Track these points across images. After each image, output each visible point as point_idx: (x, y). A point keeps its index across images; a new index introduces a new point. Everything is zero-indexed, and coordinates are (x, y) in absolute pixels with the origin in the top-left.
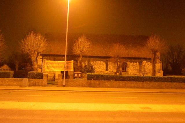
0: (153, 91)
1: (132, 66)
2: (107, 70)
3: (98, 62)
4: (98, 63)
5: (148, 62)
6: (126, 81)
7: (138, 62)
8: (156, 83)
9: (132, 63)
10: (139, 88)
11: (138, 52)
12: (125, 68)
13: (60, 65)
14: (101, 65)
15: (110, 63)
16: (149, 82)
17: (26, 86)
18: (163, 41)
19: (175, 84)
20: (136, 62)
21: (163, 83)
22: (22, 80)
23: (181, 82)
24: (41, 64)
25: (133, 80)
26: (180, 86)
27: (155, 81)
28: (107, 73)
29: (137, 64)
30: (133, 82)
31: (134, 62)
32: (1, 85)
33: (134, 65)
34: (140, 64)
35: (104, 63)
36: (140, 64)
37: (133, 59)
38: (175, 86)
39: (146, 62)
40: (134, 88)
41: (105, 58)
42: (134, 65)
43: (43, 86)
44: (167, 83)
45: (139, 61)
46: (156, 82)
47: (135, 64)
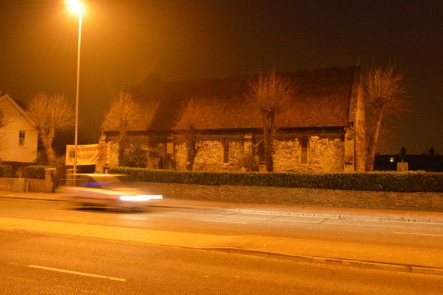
0: (183, 204)
1: (283, 148)
2: (226, 160)
3: (208, 142)
4: (207, 145)
5: (325, 137)
6: (182, 185)
7: (299, 140)
8: (248, 190)
9: (283, 143)
10: (209, 200)
11: (303, 113)
12: (265, 154)
13: (90, 153)
14: (215, 150)
15: (233, 143)
16: (231, 187)
17: (18, 192)
18: (121, 100)
19: (294, 191)
20: (293, 140)
21: (264, 189)
22: (12, 182)
23: (311, 188)
24: (353, 155)
25: (197, 182)
26: (306, 198)
27: (245, 185)
28: (226, 169)
29: (294, 144)
30: (196, 185)
31: (287, 140)
32: (0, 190)
33: (288, 148)
34: (304, 144)
35: (220, 145)
36: (304, 144)
37: (289, 132)
38: (293, 196)
39: (317, 137)
40: (199, 200)
41: (225, 134)
42: (288, 148)
43: (45, 192)
44: (274, 188)
45: (301, 135)
46: (247, 187)
47: (290, 143)
